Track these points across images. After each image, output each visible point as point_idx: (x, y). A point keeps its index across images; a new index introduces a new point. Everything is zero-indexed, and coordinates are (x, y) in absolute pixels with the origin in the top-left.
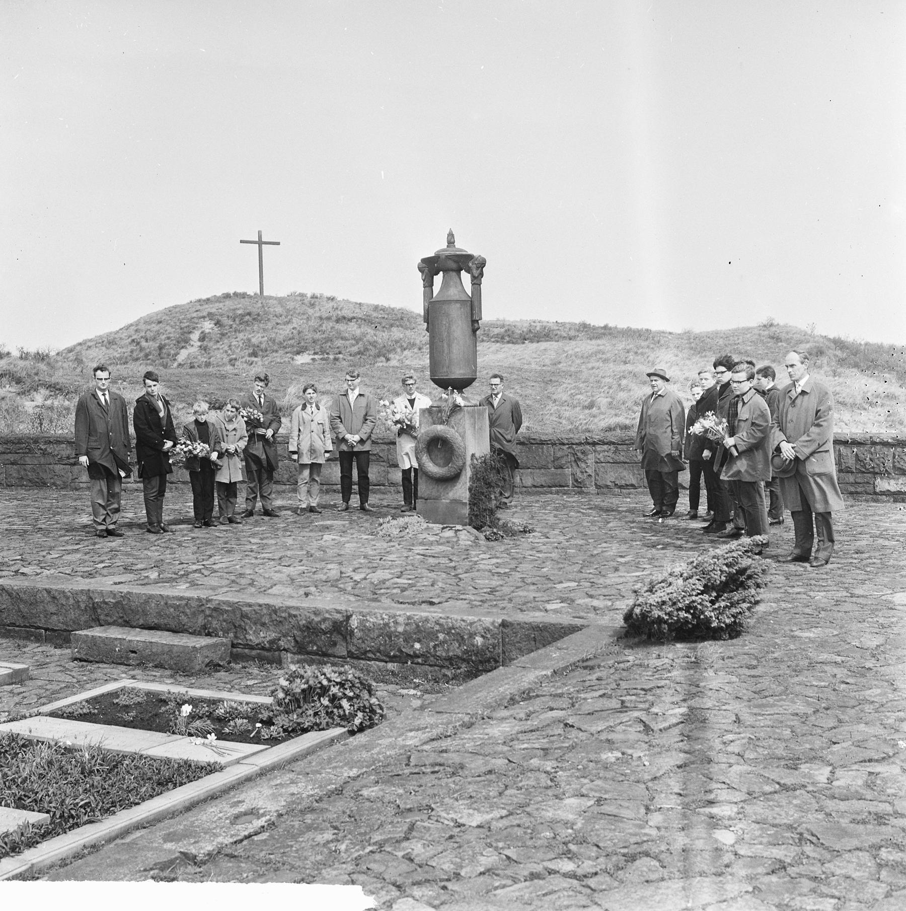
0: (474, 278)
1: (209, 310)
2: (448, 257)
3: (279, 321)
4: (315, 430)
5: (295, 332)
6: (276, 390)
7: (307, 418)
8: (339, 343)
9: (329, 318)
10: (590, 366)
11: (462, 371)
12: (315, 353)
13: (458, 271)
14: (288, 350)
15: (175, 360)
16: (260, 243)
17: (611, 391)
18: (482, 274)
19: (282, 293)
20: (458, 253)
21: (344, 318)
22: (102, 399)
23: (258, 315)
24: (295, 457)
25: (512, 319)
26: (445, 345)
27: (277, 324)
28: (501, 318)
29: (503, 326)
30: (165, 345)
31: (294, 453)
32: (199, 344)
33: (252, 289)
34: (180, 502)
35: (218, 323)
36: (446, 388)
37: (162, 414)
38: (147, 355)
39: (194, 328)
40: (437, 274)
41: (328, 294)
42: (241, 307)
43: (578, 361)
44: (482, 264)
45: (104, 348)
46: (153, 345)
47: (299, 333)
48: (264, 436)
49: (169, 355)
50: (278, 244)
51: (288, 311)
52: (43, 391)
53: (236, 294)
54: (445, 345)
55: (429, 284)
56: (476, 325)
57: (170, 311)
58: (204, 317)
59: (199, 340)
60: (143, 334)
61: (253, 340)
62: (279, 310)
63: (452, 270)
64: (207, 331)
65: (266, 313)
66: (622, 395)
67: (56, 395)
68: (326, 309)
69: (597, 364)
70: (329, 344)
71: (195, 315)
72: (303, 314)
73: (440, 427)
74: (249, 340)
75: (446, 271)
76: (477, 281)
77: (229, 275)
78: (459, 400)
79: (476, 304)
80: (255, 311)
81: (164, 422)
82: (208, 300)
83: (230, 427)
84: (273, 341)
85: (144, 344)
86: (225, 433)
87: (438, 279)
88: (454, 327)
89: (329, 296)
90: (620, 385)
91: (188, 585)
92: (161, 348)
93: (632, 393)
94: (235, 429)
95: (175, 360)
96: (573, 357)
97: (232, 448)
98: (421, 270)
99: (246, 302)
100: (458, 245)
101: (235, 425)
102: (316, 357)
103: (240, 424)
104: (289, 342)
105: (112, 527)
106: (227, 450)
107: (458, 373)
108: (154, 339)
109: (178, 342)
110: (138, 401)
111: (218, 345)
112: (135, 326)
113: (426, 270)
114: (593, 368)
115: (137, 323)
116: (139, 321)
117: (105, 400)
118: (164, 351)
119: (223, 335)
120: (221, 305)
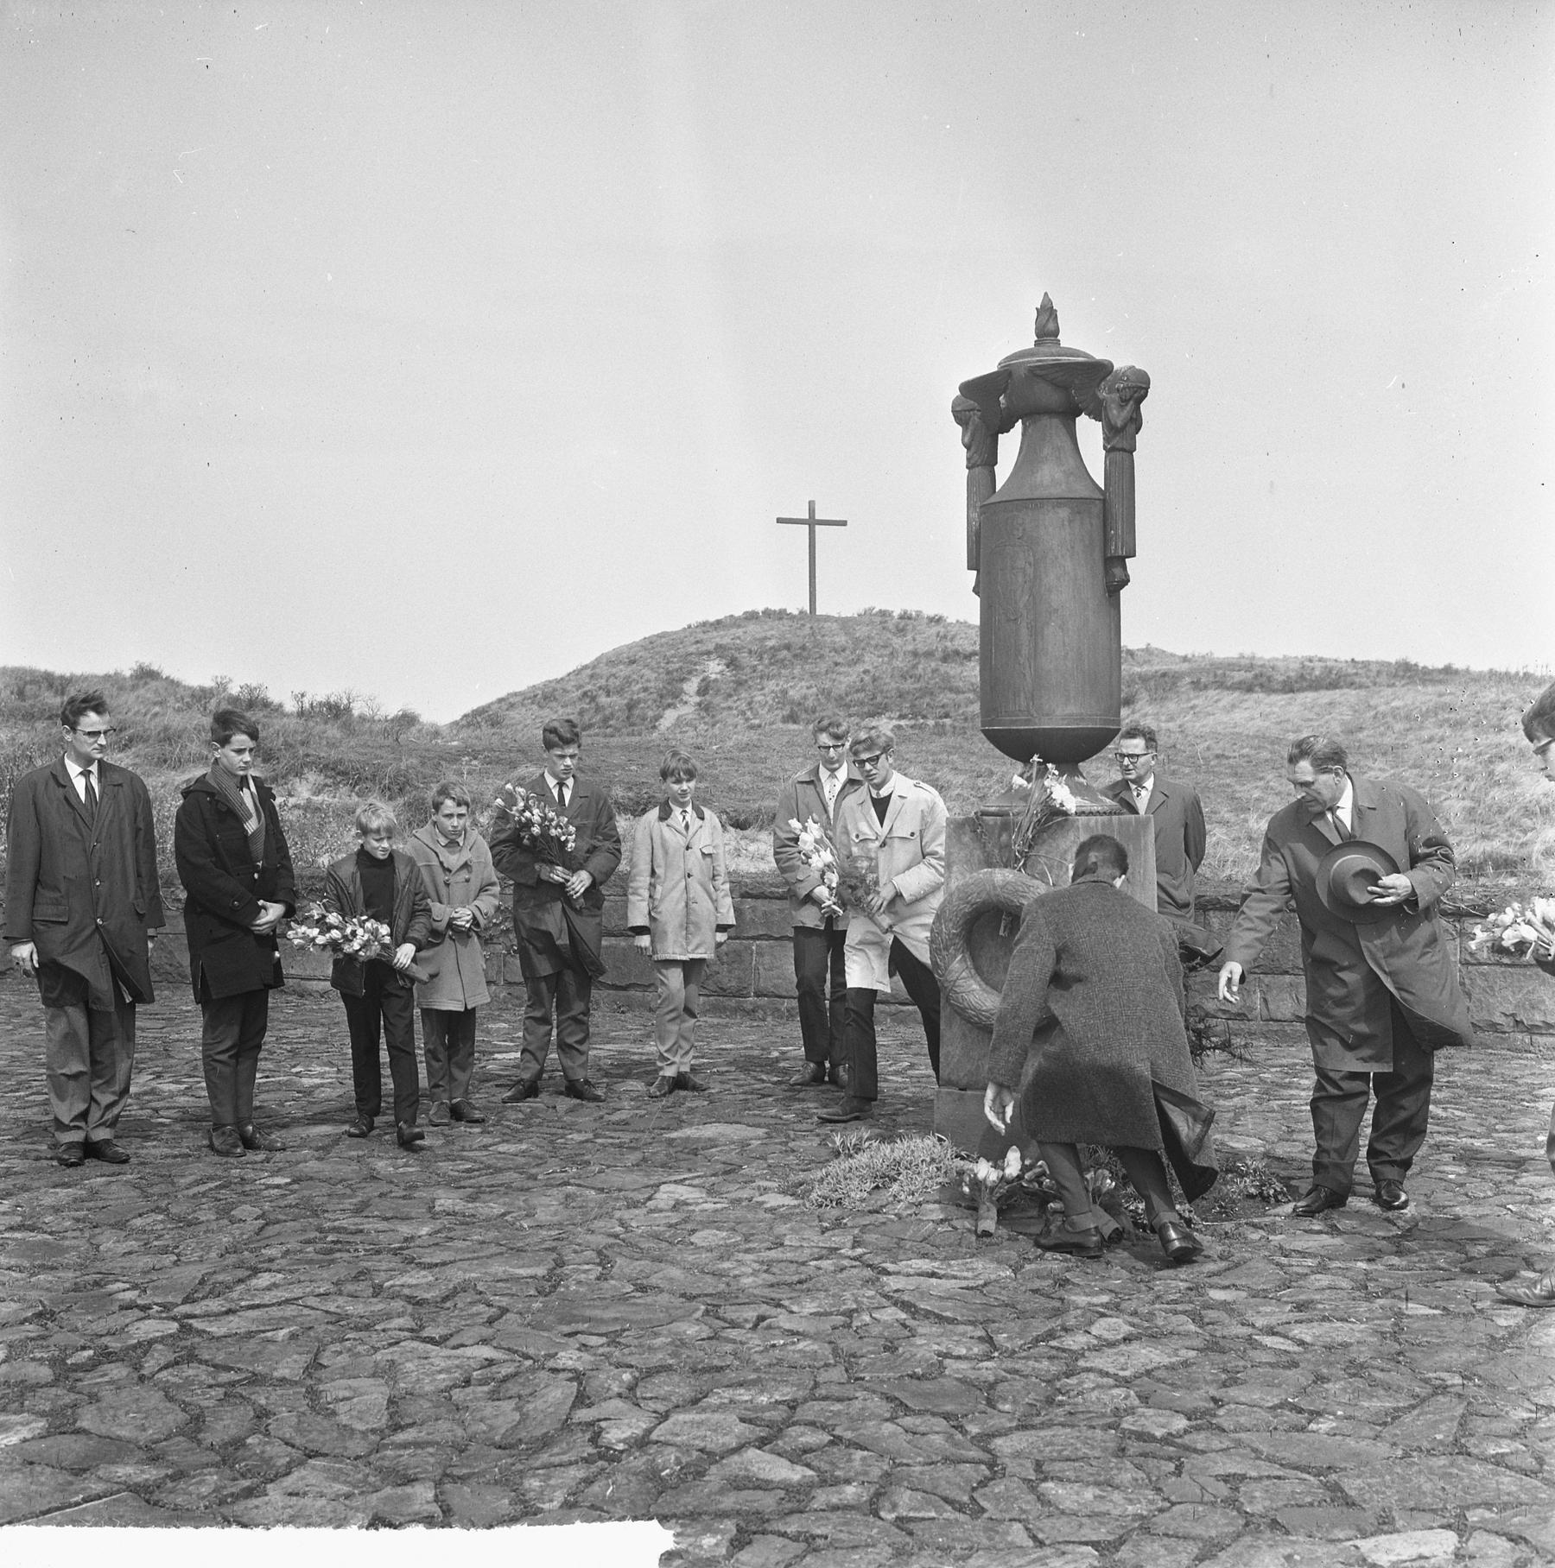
0: (1111, 432)
1: (718, 640)
2: (1039, 373)
3: (840, 660)
4: (695, 872)
5: (867, 678)
6: (771, 779)
7: (675, 841)
8: (946, 698)
9: (929, 654)
10: (1425, 734)
11: (1072, 709)
12: (902, 717)
13: (1069, 415)
14: (853, 710)
15: (654, 727)
16: (812, 522)
17: (1473, 786)
18: (1136, 422)
19: (850, 610)
20: (1065, 359)
21: (957, 653)
22: (80, 785)
23: (803, 648)
24: (644, 941)
25: (1267, 656)
26: (1024, 632)
27: (837, 664)
28: (1247, 653)
29: (1251, 667)
30: (639, 701)
31: (641, 930)
32: (698, 699)
33: (796, 603)
34: (309, 1057)
35: (732, 663)
36: (1025, 759)
37: (251, 826)
38: (606, 720)
39: (690, 672)
40: (1006, 428)
41: (929, 611)
42: (774, 635)
43: (1399, 726)
44: (1137, 388)
45: (535, 707)
46: (618, 702)
47: (874, 680)
48: (562, 887)
49: (644, 719)
50: (844, 523)
51: (857, 641)
52: (313, 777)
53: (768, 613)
54: (1024, 632)
55: (982, 456)
56: (1117, 571)
57: (651, 643)
58: (708, 653)
59: (699, 693)
60: (603, 682)
61: (791, 693)
62: (841, 639)
63: (1049, 412)
64: (713, 676)
65: (817, 645)
66: (1497, 794)
67: (336, 784)
68: (926, 638)
69: (1439, 732)
70: (927, 700)
71: (692, 649)
72: (885, 647)
73: (1002, 876)
74: (784, 692)
75: (1030, 414)
76: (1121, 440)
77: (756, 580)
78: (1062, 794)
79: (1117, 509)
80: (797, 641)
81: (259, 847)
82: (718, 624)
83: (453, 860)
84: (826, 693)
85: (603, 700)
86: (441, 877)
87: (1010, 444)
88: (1050, 579)
89: (932, 614)
90: (1491, 773)
91: (41, 1424)
92: (631, 707)
93: (1518, 790)
94: (466, 866)
95: (654, 727)
96: (1389, 719)
97: (463, 916)
98: (960, 416)
99: (784, 626)
100: (1067, 340)
101: (465, 856)
102: (903, 723)
103: (478, 850)
104: (856, 696)
105: (102, 1134)
106: (450, 925)
107: (1062, 712)
108: (620, 691)
109: (662, 697)
110: (186, 794)
111: (730, 703)
112: (591, 671)
113: (976, 418)
114: (1431, 740)
115: (594, 665)
116: (598, 660)
117: (89, 788)
118: (637, 712)
119: (740, 683)
120: (740, 632)
